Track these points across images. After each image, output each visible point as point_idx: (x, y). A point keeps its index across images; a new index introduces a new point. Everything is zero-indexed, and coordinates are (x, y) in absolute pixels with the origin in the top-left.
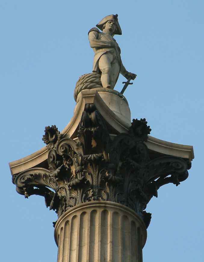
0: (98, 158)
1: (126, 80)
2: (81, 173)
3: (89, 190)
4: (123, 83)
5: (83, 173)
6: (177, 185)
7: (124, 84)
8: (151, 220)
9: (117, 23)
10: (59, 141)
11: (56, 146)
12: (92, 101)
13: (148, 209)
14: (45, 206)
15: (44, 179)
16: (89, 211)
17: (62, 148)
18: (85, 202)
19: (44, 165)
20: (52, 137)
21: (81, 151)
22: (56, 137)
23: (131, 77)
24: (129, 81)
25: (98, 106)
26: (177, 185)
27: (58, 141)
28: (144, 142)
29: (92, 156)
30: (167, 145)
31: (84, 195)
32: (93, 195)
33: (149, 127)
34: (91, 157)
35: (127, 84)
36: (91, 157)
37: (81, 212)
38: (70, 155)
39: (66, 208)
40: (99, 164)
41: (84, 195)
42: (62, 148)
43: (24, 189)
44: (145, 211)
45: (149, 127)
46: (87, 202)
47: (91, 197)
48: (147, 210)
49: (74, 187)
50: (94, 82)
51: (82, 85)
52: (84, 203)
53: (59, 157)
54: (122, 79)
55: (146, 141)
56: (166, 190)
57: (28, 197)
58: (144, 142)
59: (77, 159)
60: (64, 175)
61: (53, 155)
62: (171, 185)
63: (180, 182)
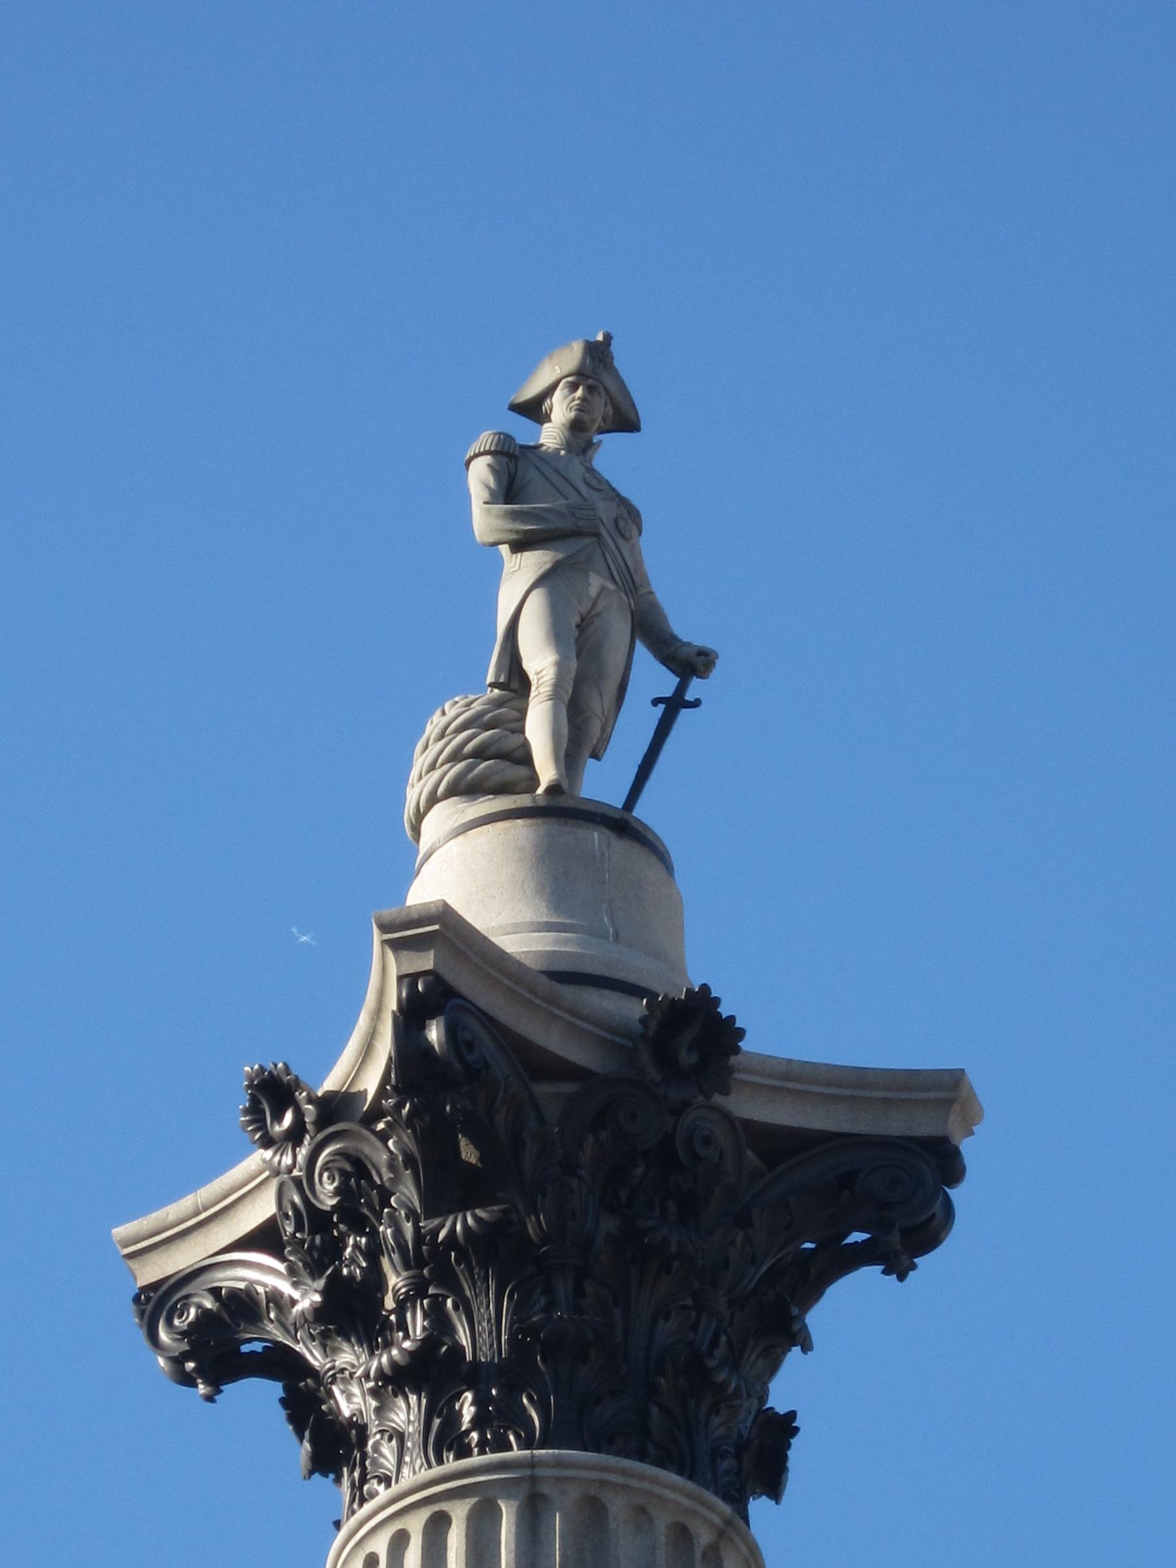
0: (408, 1358)
1: (667, 683)
2: (422, 1304)
3: (458, 1396)
4: (656, 702)
5: (425, 1302)
6: (902, 1277)
7: (662, 707)
8: (790, 1464)
9: (610, 383)
10: (312, 1138)
11: (303, 1152)
12: (426, 961)
13: (781, 1395)
14: (294, 1438)
15: (272, 1315)
16: (459, 1512)
17: (326, 1175)
18: (440, 1461)
19: (265, 1238)
20: (278, 1118)
21: (407, 1192)
22: (299, 1115)
23: (690, 664)
24: (681, 689)
25: (463, 980)
26: (902, 1277)
27: (308, 1137)
28: (718, 1099)
29: (459, 1224)
30: (840, 1086)
31: (437, 1422)
32: (476, 1423)
33: (732, 1019)
34: (453, 1229)
35: (674, 705)
36: (453, 1229)
37: (424, 1514)
38: (365, 1211)
39: (366, 1488)
40: (493, 1250)
41: (437, 1422)
42: (326, 1175)
43: (190, 1365)
44: (771, 1408)
45: (732, 1019)
46: (452, 1464)
47: (468, 1432)
48: (781, 1395)
49: (393, 1382)
50: (488, 753)
51: (436, 774)
52: (437, 1471)
53: (315, 1219)
54: (651, 678)
55: (725, 1091)
56: (853, 1309)
57: (216, 1397)
58: (718, 1099)
59: (398, 1233)
60: (351, 1312)
61: (293, 1205)
62: (869, 1276)
63: (915, 1260)
